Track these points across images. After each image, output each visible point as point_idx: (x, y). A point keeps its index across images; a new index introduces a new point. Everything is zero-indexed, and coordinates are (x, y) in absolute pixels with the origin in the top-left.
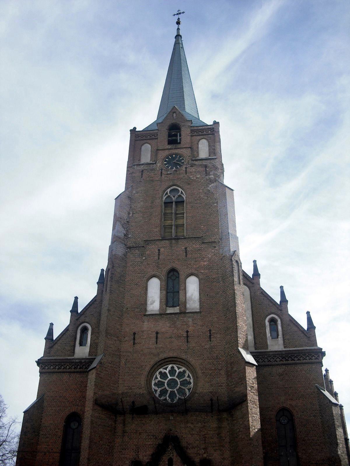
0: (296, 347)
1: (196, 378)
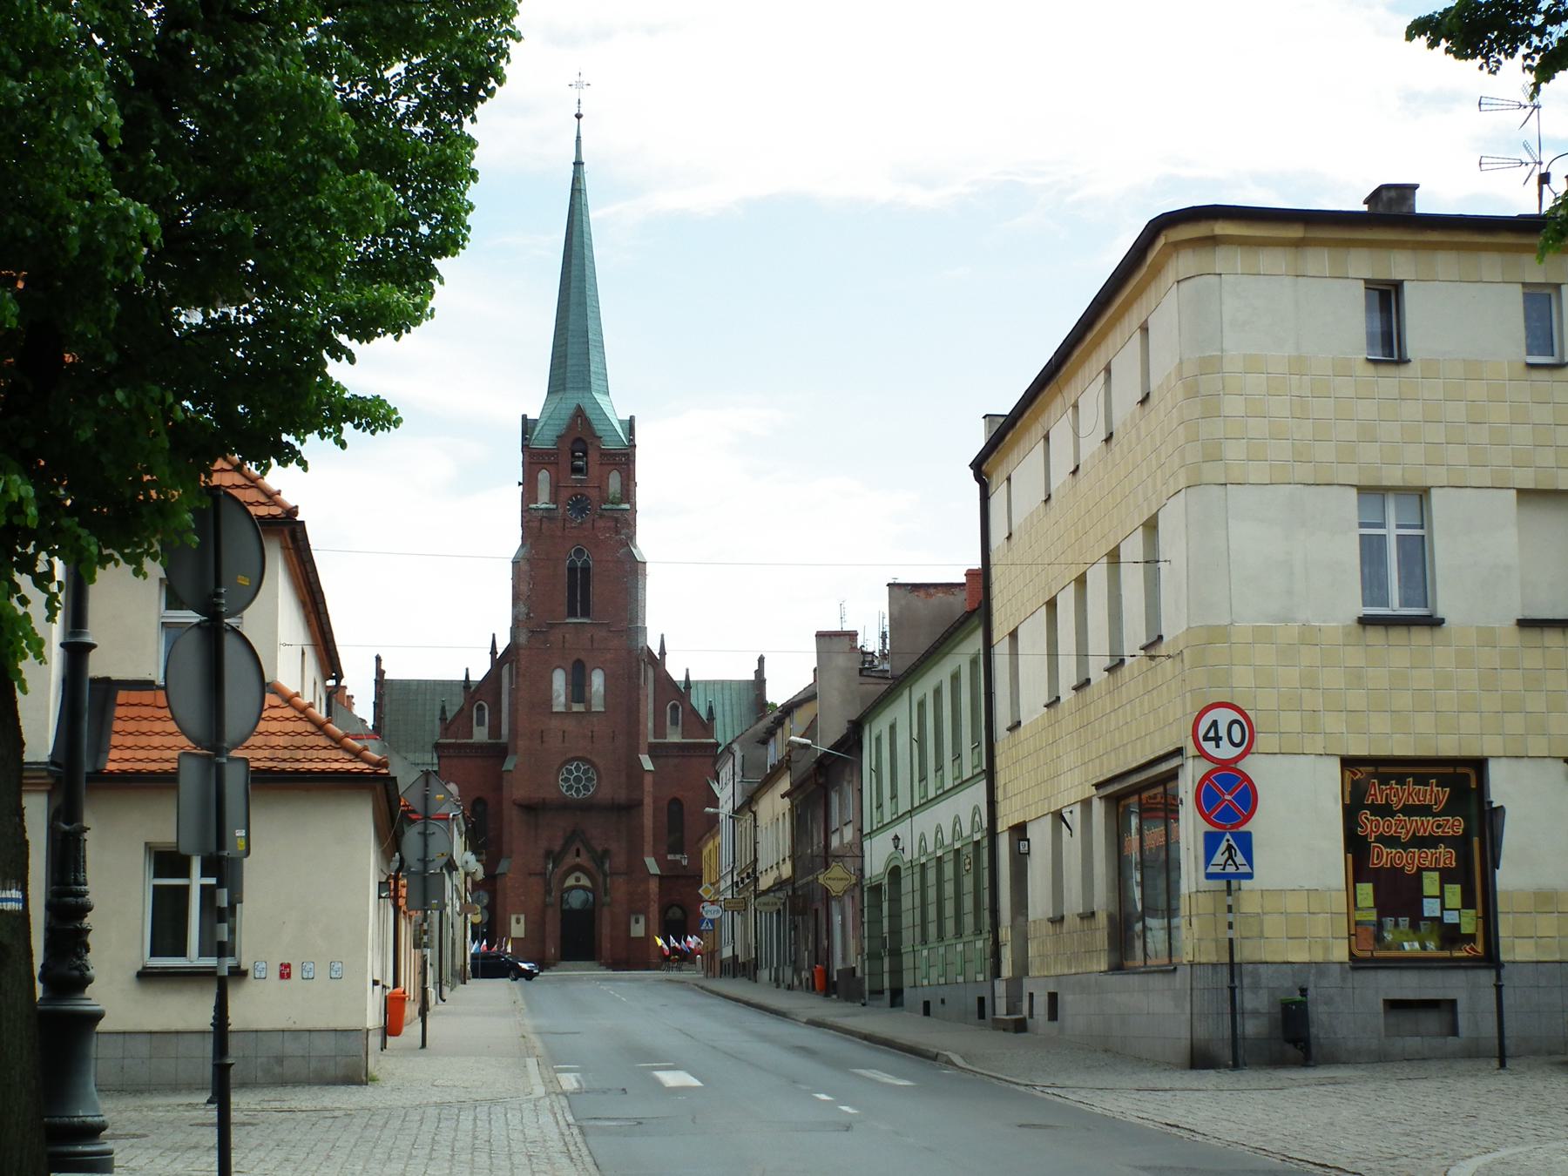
1: (599, 778)
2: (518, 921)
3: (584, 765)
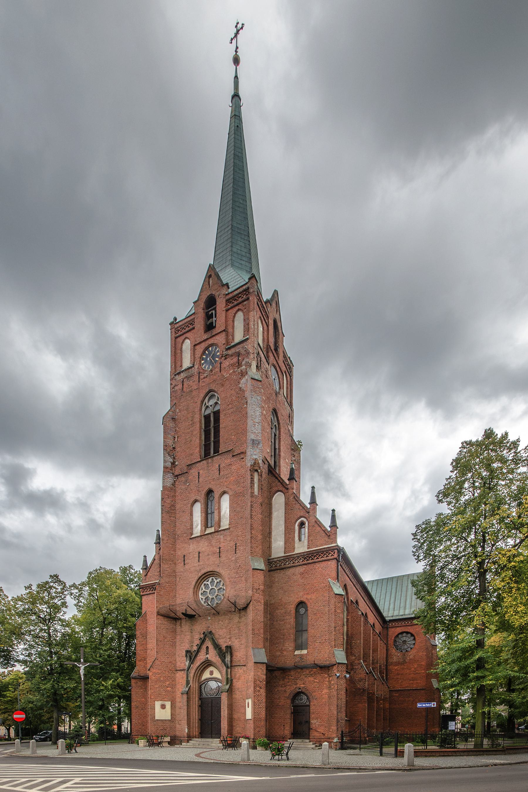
0: (317, 546)
2: (163, 707)
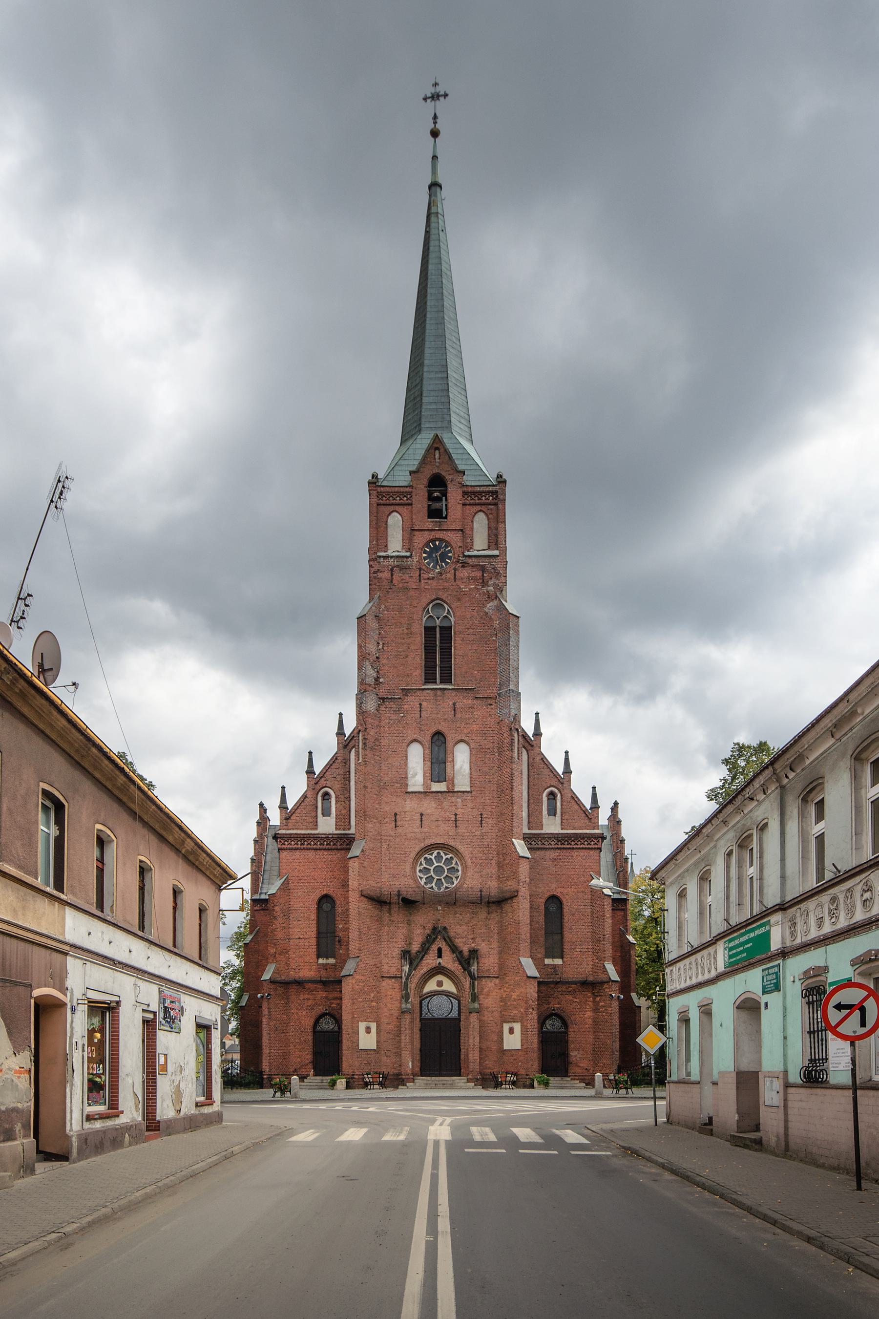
0: (575, 829)
2: (368, 1030)
3: (446, 854)
